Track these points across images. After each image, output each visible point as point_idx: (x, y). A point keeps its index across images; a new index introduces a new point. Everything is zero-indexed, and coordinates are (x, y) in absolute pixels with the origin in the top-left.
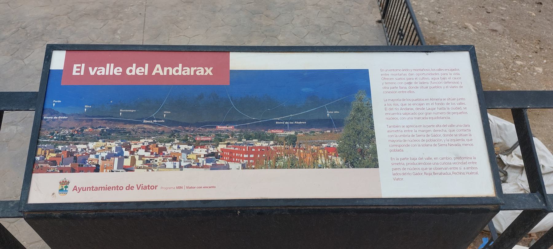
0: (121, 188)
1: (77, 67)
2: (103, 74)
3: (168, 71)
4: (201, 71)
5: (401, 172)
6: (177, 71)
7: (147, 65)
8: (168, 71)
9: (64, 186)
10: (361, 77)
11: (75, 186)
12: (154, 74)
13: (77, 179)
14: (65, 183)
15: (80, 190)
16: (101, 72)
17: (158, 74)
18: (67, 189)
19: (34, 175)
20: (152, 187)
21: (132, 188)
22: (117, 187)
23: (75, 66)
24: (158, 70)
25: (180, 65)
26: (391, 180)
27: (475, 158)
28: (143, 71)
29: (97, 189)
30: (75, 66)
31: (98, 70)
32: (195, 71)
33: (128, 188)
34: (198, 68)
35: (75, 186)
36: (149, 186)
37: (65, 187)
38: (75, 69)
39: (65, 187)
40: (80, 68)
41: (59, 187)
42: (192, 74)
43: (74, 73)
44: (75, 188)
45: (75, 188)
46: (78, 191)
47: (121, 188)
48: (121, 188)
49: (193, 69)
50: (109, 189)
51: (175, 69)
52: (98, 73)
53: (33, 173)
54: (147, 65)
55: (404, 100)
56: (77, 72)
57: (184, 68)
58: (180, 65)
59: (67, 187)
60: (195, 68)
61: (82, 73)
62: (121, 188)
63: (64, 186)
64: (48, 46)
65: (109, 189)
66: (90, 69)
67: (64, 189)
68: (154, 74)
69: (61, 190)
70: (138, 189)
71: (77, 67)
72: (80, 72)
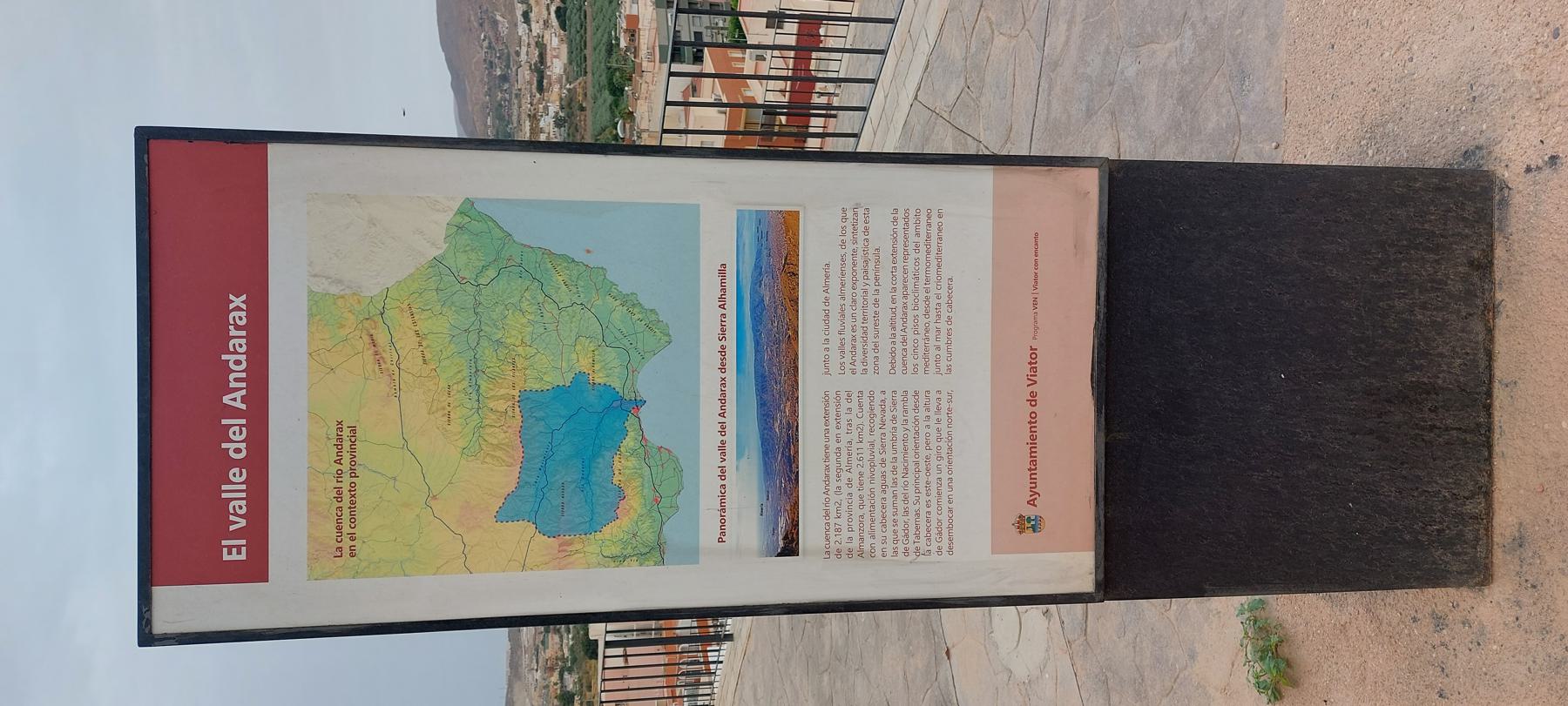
0: (1033, 416)
1: (230, 553)
2: (243, 341)
7: (224, 422)
12: (243, 407)
17: (244, 400)
23: (226, 557)
29: (1033, 462)
30: (226, 557)
31: (236, 514)
32: (237, 328)
38: (235, 557)
40: (230, 548)
41: (1029, 534)
42: (243, 333)
43: (243, 557)
45: (1032, 503)
49: (233, 332)
50: (1033, 438)
51: (232, 365)
54: (224, 422)
56: (239, 553)
61: (243, 542)
62: (1033, 416)
65: (1033, 438)
66: (232, 528)
68: (243, 407)
69: (1034, 529)
71: (230, 553)
72: (239, 547)
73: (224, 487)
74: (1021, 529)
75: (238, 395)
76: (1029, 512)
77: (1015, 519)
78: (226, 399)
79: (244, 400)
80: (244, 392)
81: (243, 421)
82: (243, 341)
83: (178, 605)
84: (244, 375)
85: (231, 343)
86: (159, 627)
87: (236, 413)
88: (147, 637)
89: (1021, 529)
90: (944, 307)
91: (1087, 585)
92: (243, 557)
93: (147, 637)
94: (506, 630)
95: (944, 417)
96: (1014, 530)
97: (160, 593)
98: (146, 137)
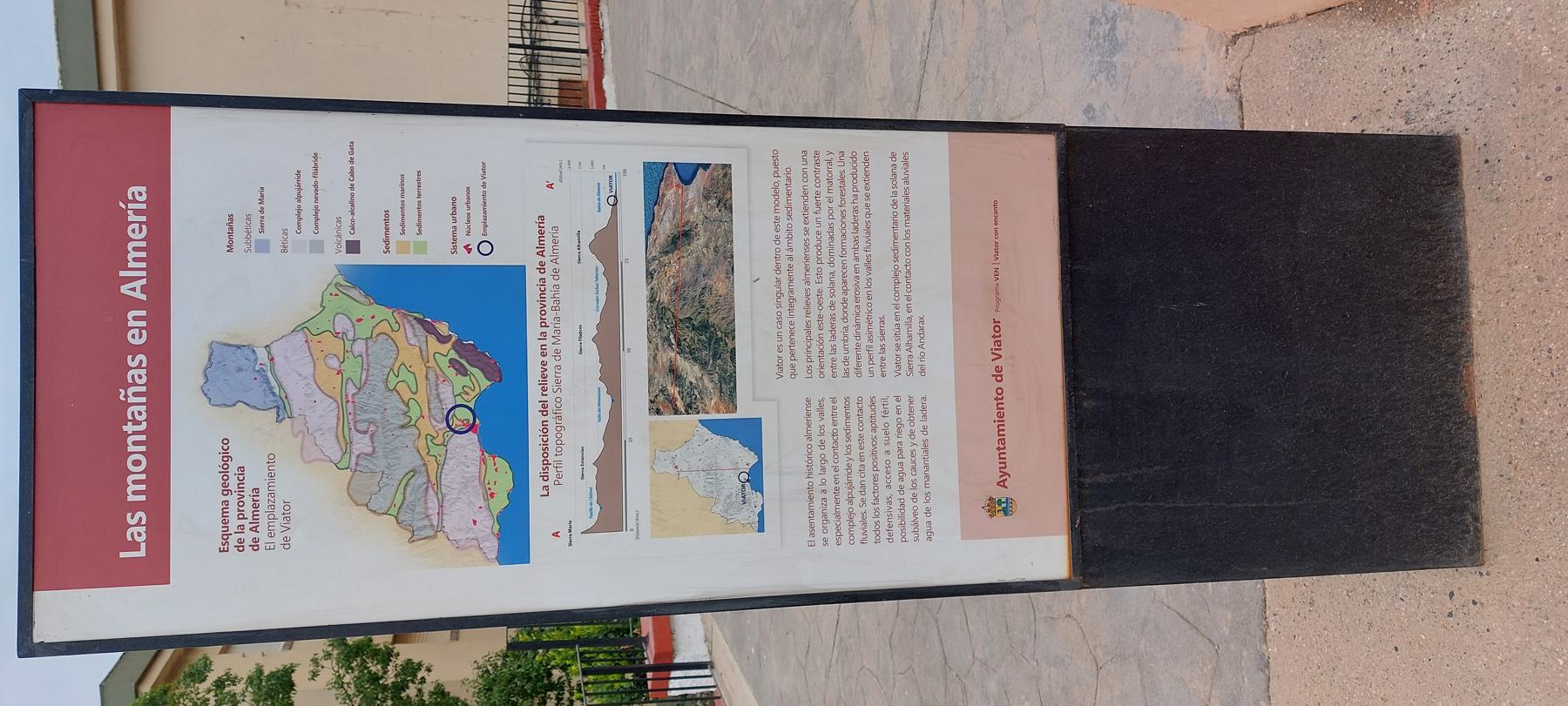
2: (143, 409)
12: (144, 297)
17: (144, 289)
19: (36, 594)
21: (999, 370)
24: (134, 289)
28: (136, 226)
29: (1002, 440)
30: (143, 189)
42: (144, 218)
44: (1002, 484)
45: (1002, 484)
50: (1001, 416)
65: (1001, 416)
68: (144, 297)
69: (1006, 512)
73: (122, 274)
74: (992, 512)
75: (138, 284)
76: (999, 493)
77: (984, 502)
78: (124, 289)
79: (144, 289)
80: (144, 281)
81: (144, 218)
82: (143, 409)
83: (60, 612)
84: (144, 389)
85: (130, 373)
86: (41, 634)
87: (137, 304)
88: (28, 647)
89: (992, 512)
90: (863, 269)
91: (1059, 566)
92: (142, 553)
93: (28, 647)
95: (784, 264)
96: (985, 514)
97: (41, 598)
98: (24, 93)
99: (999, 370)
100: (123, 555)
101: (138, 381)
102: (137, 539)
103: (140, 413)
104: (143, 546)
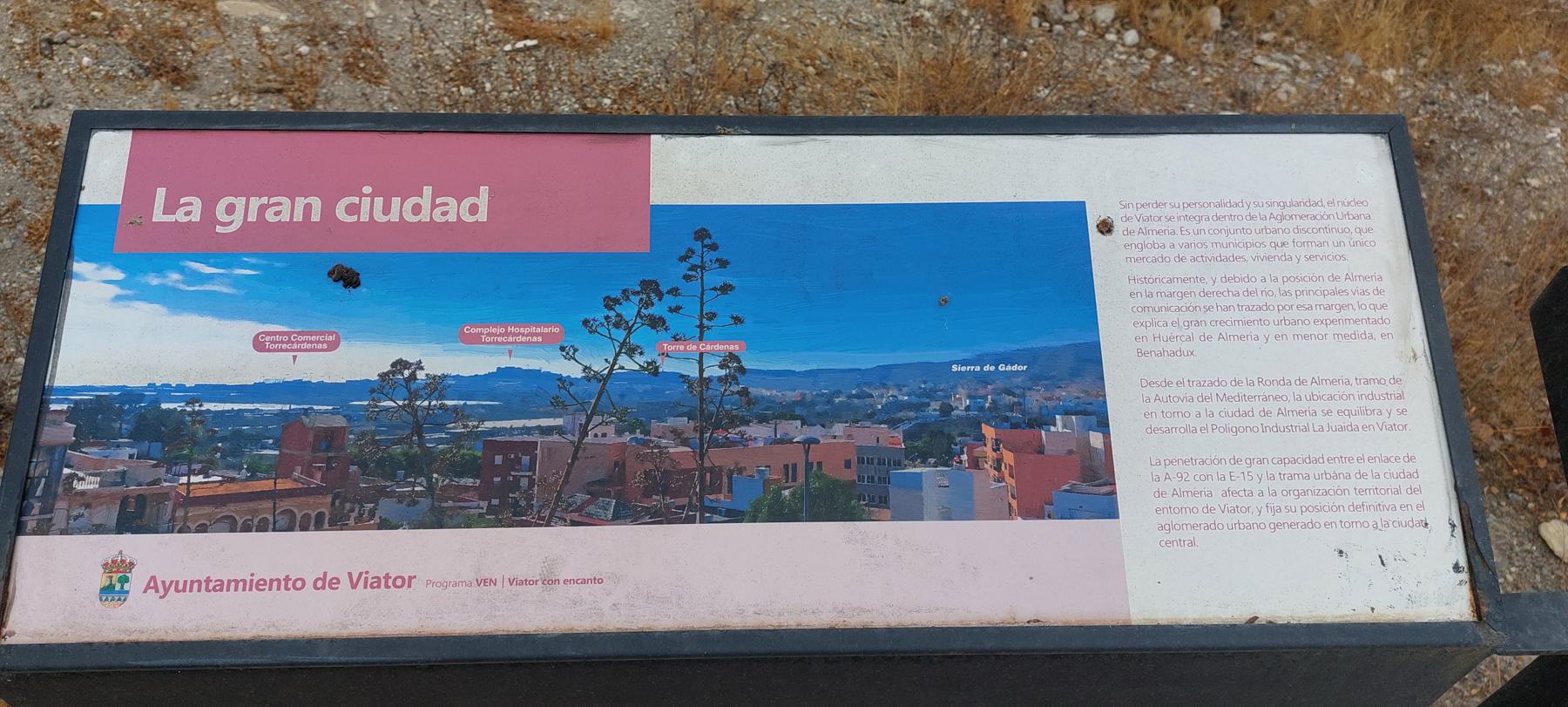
0: (297, 584)
2: (285, 217)
3: (387, 210)
4: (453, 210)
5: (1201, 518)
6: (417, 209)
8: (387, 210)
9: (116, 577)
10: (1054, 243)
11: (153, 578)
13: (150, 552)
14: (119, 569)
15: (166, 591)
16: (277, 213)
18: (126, 587)
20: (399, 582)
21: (334, 583)
22: (287, 579)
25: (428, 191)
26: (1173, 556)
27: (1411, 459)
29: (221, 586)
30: (482, 216)
32: (262, 209)
33: (320, 584)
34: (274, 200)
35: (153, 578)
36: (387, 577)
37: (120, 580)
39: (120, 580)
41: (101, 580)
44: (152, 584)
45: (152, 584)
46: (162, 592)
47: (299, 584)
48: (299, 584)
49: (255, 203)
50: (260, 585)
51: (413, 200)
52: (270, 216)
53: (20, 529)
55: (1238, 383)
57: (438, 201)
58: (428, 191)
59: (127, 580)
60: (264, 200)
62: (297, 584)
63: (116, 577)
64: (78, 118)
67: (118, 587)
69: (107, 590)
70: (354, 586)
92: (158, 216)
94: (130, 133)
99: (334, 583)
100: (161, 193)
101: (438, 211)
102: (182, 210)
103: (445, 214)
104: (170, 218)
